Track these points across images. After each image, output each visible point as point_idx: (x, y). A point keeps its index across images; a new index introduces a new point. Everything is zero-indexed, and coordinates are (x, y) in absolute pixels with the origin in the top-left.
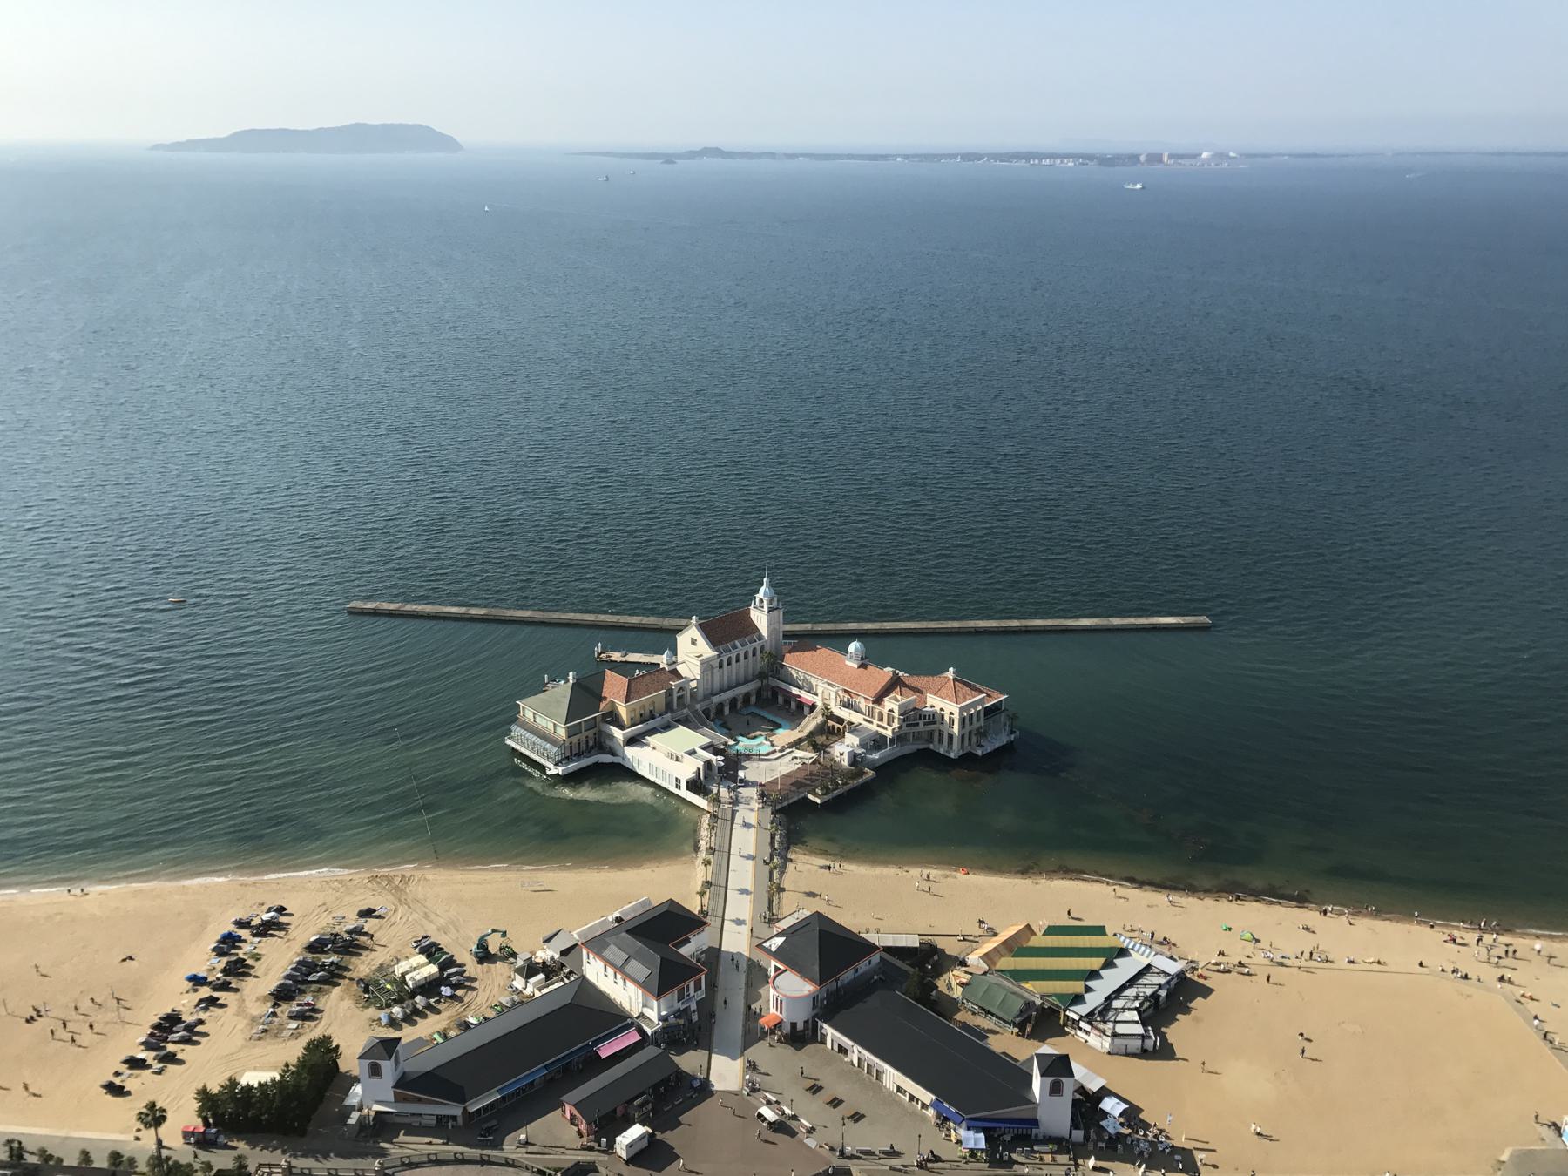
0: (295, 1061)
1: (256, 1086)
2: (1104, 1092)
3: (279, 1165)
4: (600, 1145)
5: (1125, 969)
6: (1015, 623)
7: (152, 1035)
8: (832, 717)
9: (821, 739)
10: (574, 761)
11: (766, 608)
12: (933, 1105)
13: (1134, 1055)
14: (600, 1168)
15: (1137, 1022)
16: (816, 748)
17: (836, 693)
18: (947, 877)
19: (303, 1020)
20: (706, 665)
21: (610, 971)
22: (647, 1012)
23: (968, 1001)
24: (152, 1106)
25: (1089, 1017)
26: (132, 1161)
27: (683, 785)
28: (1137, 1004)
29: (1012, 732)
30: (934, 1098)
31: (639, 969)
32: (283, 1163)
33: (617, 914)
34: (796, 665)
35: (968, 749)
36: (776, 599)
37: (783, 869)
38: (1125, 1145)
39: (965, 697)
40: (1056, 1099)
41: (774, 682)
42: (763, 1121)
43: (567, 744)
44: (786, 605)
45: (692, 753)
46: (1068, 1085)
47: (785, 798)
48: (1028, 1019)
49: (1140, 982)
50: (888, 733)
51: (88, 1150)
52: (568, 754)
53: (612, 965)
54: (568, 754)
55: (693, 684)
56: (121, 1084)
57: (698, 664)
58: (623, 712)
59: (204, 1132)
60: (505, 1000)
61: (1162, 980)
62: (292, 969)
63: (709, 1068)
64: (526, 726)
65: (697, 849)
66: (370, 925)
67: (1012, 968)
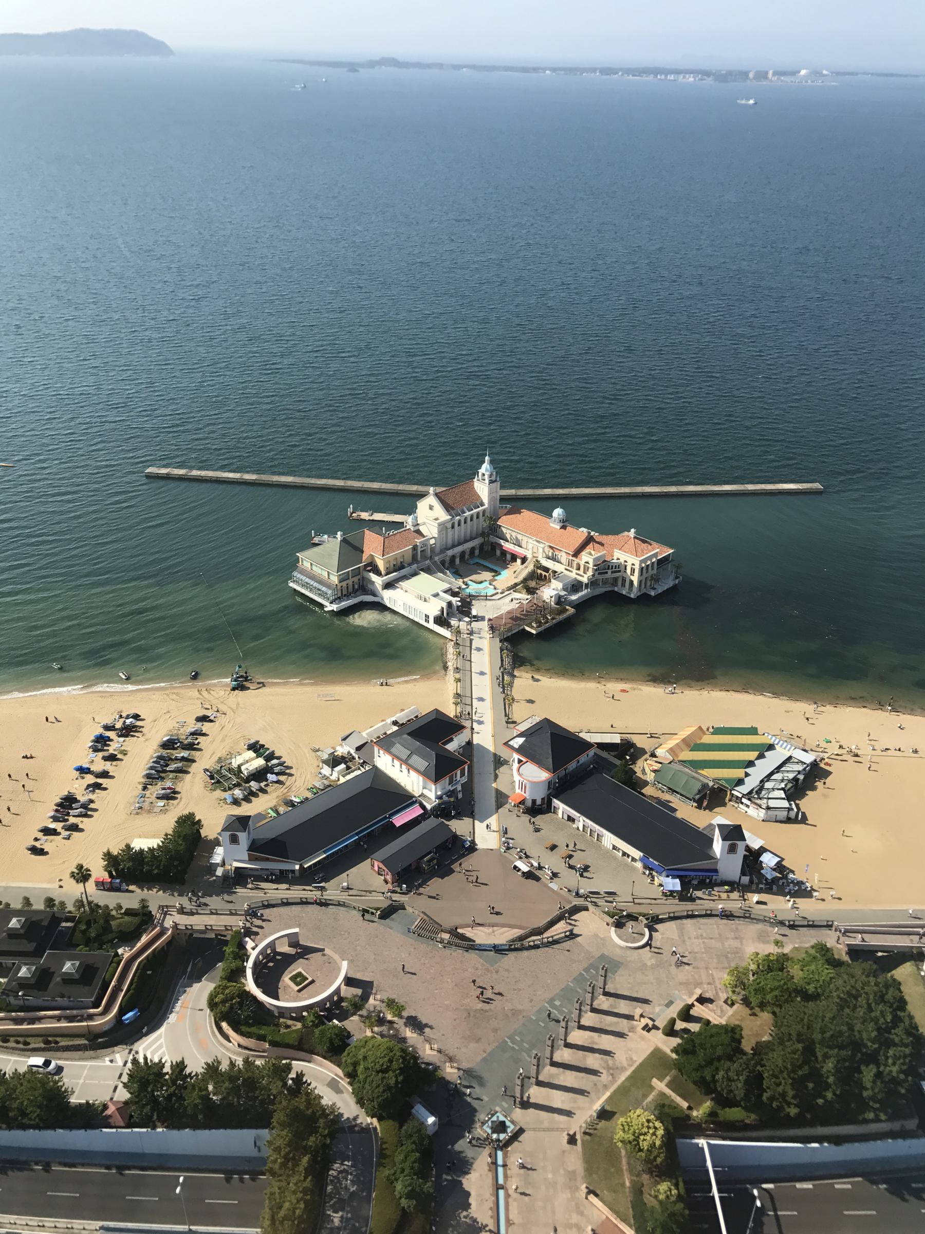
0: (171, 832)
1: (146, 850)
2: (762, 850)
3: (174, 907)
4: (401, 890)
5: (772, 760)
6: (673, 489)
7: (57, 811)
8: (538, 566)
9: (532, 584)
10: (344, 601)
11: (487, 481)
12: (641, 860)
13: (781, 822)
14: (407, 907)
15: (784, 799)
16: (531, 591)
17: (543, 548)
18: (634, 689)
19: (167, 800)
20: (442, 527)
21: (397, 763)
22: (426, 792)
23: (659, 783)
24: (80, 867)
25: (749, 795)
26: (62, 904)
27: (431, 620)
28: (783, 785)
29: (677, 578)
30: (642, 854)
31: (422, 764)
32: (177, 905)
33: (394, 719)
34: (509, 525)
35: (644, 591)
36: (494, 473)
37: (511, 684)
38: (778, 886)
39: (643, 551)
40: (732, 856)
41: (493, 539)
42: (518, 871)
43: (339, 587)
44: (502, 476)
45: (436, 595)
46: (741, 846)
47: (510, 630)
48: (704, 797)
49: (783, 769)
50: (585, 580)
51: (28, 896)
52: (339, 595)
53: (398, 758)
54: (339, 595)
55: (432, 542)
56: (42, 847)
57: (436, 525)
58: (381, 565)
59: (111, 882)
60: (318, 784)
61: (800, 767)
62: (153, 762)
63: (474, 833)
64: (303, 572)
65: (446, 668)
66: (206, 727)
67: (691, 759)
